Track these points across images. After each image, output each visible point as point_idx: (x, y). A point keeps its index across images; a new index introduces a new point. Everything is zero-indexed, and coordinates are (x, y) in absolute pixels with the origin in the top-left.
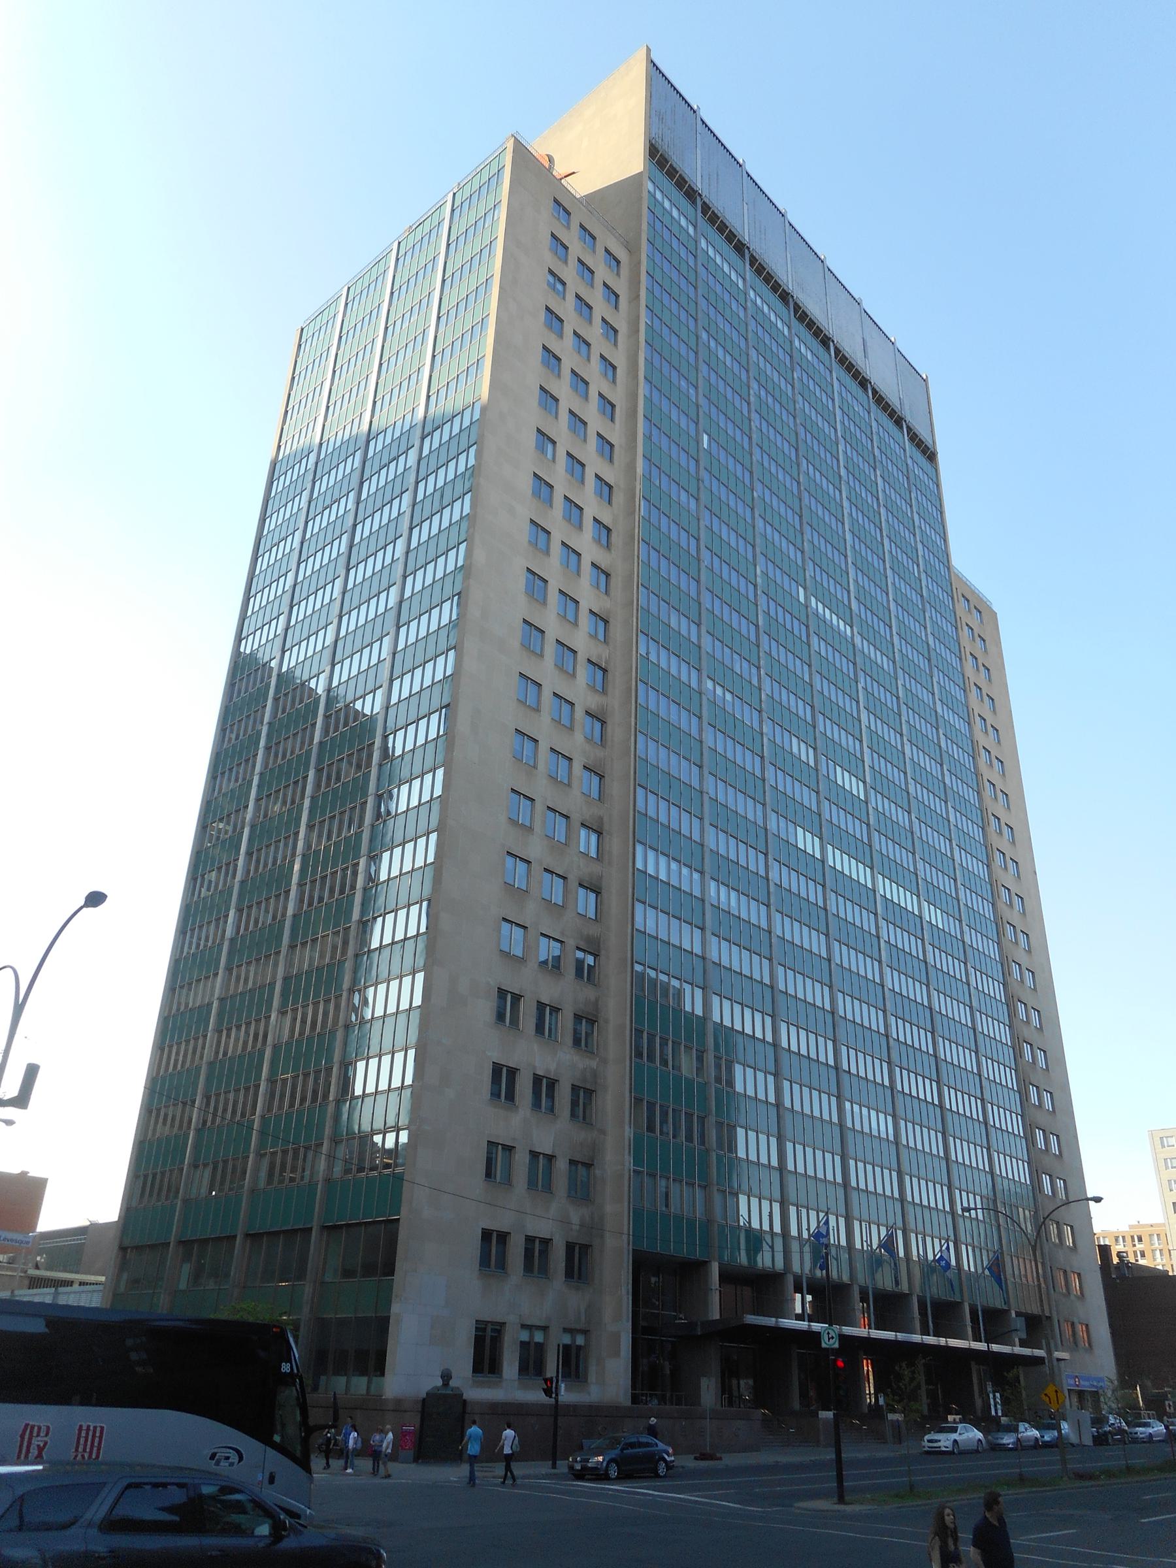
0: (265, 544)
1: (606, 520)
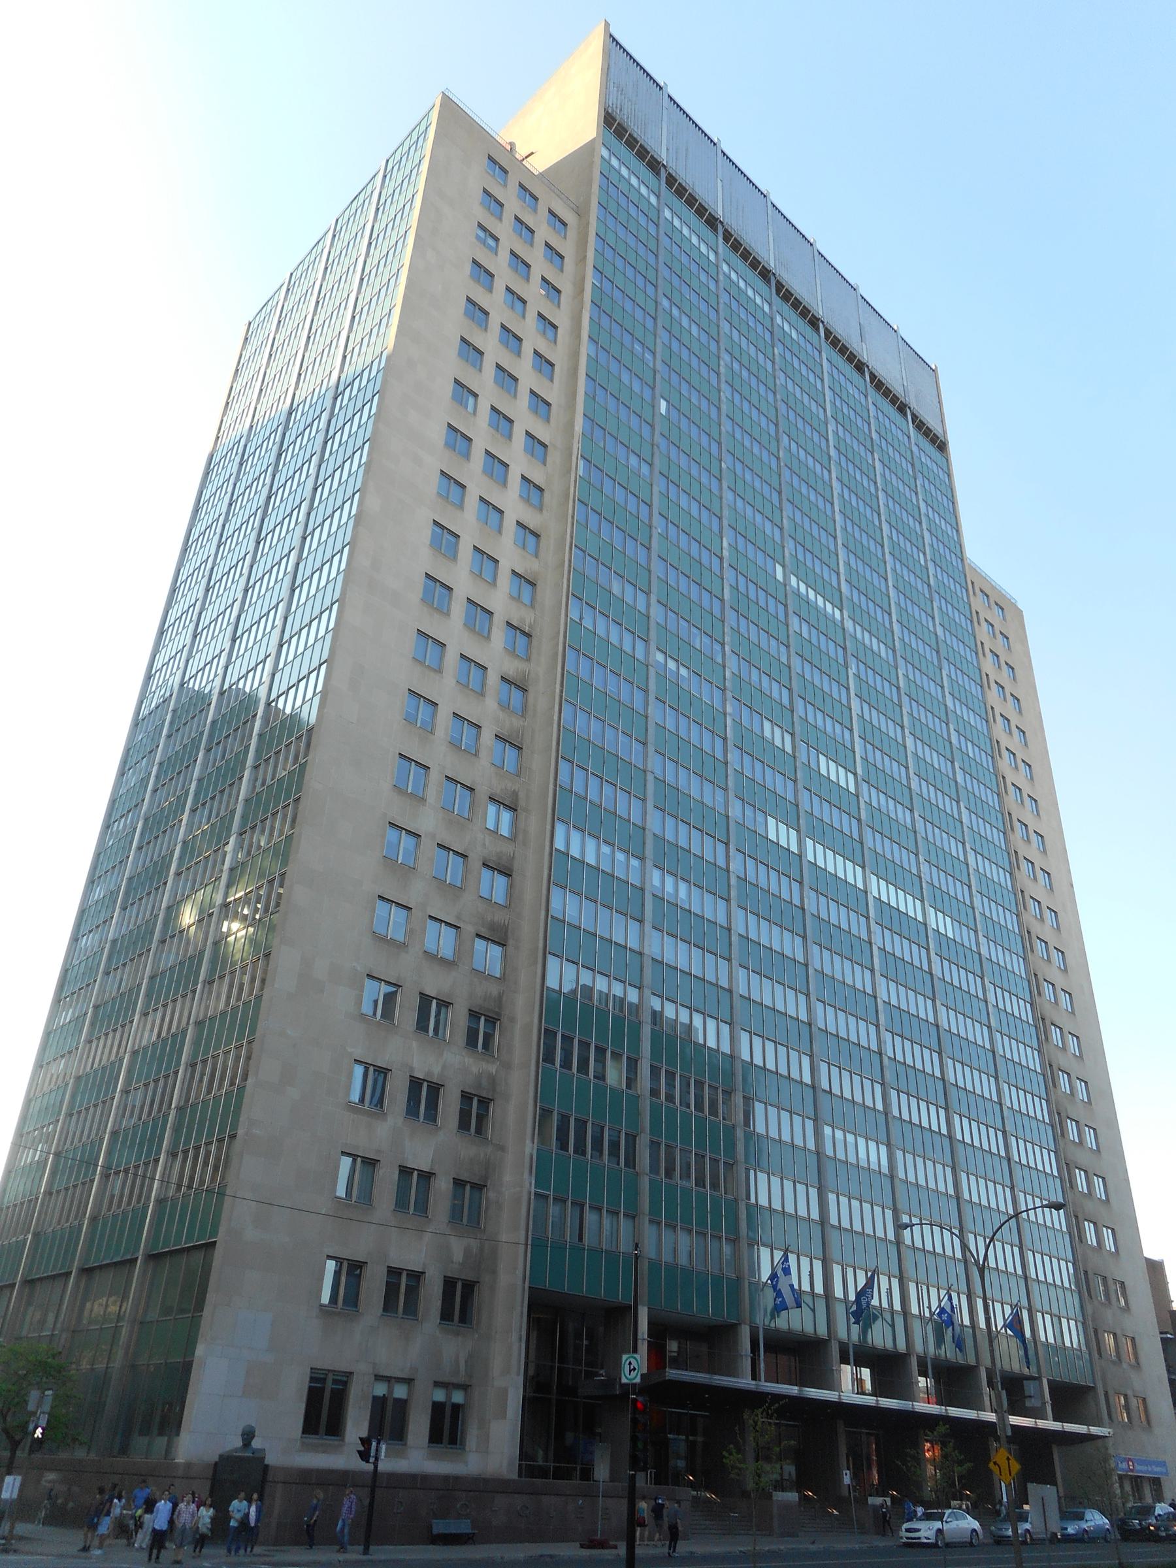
1: (538, 477)
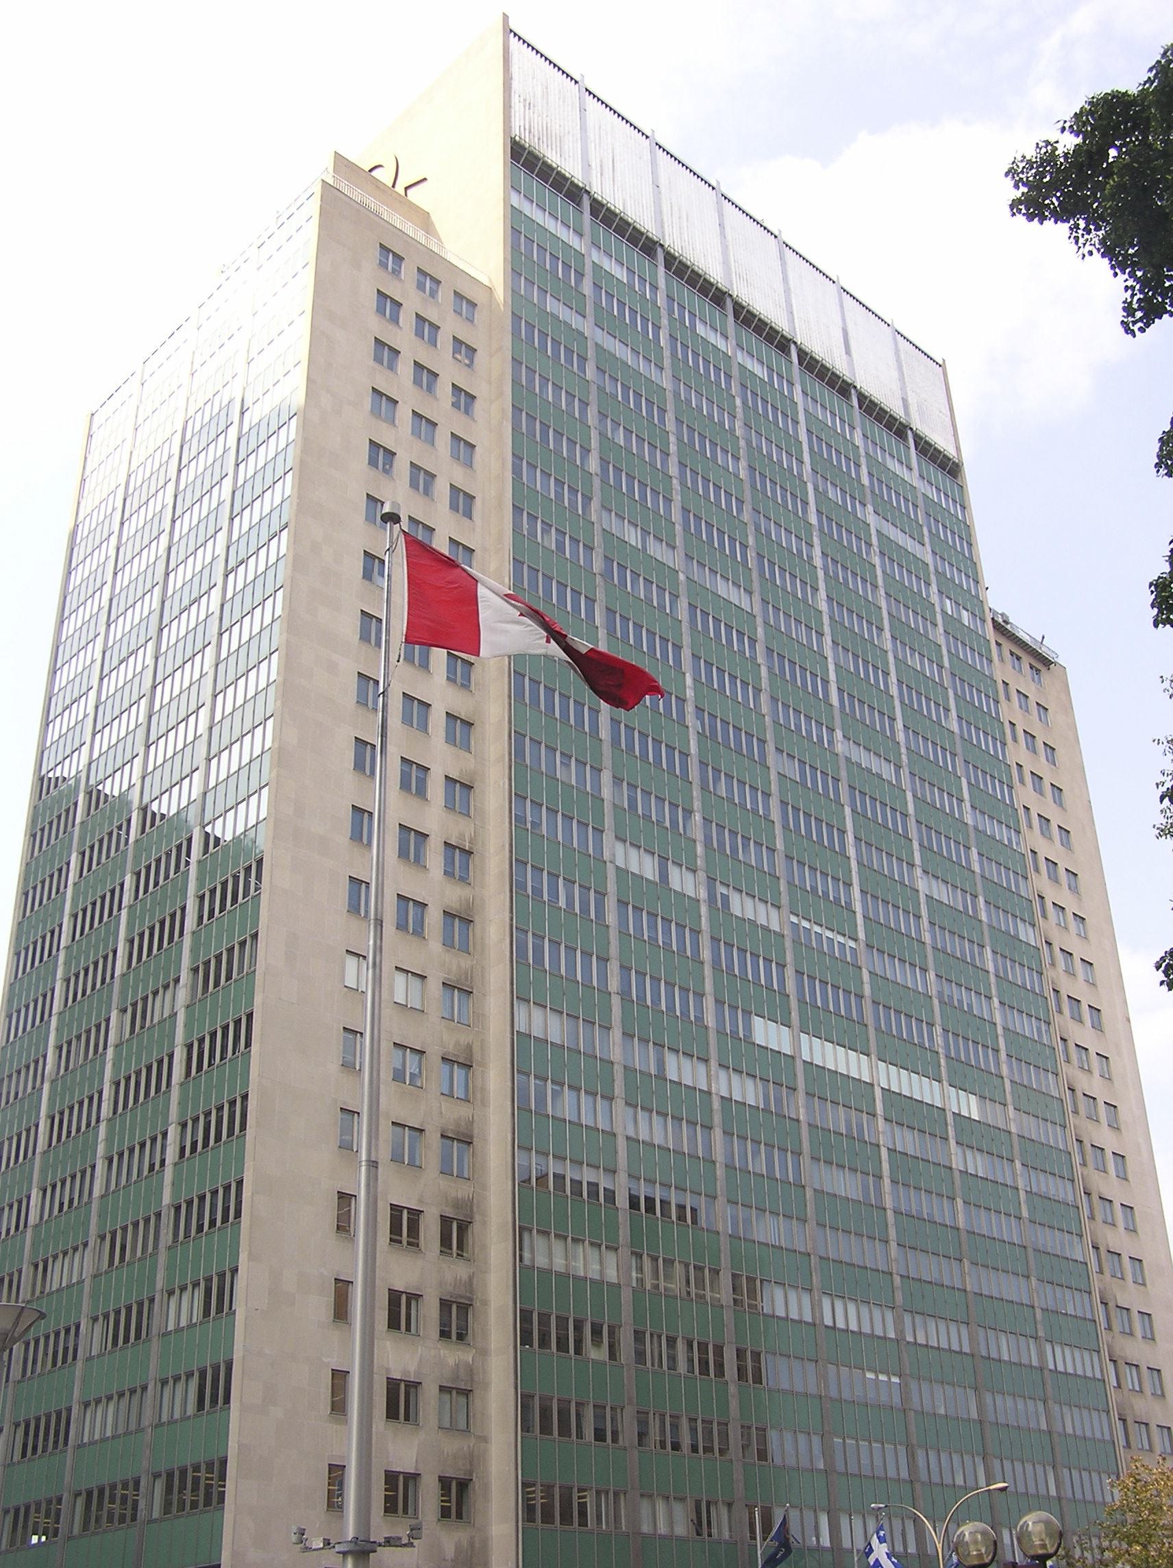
0: (78, 555)
